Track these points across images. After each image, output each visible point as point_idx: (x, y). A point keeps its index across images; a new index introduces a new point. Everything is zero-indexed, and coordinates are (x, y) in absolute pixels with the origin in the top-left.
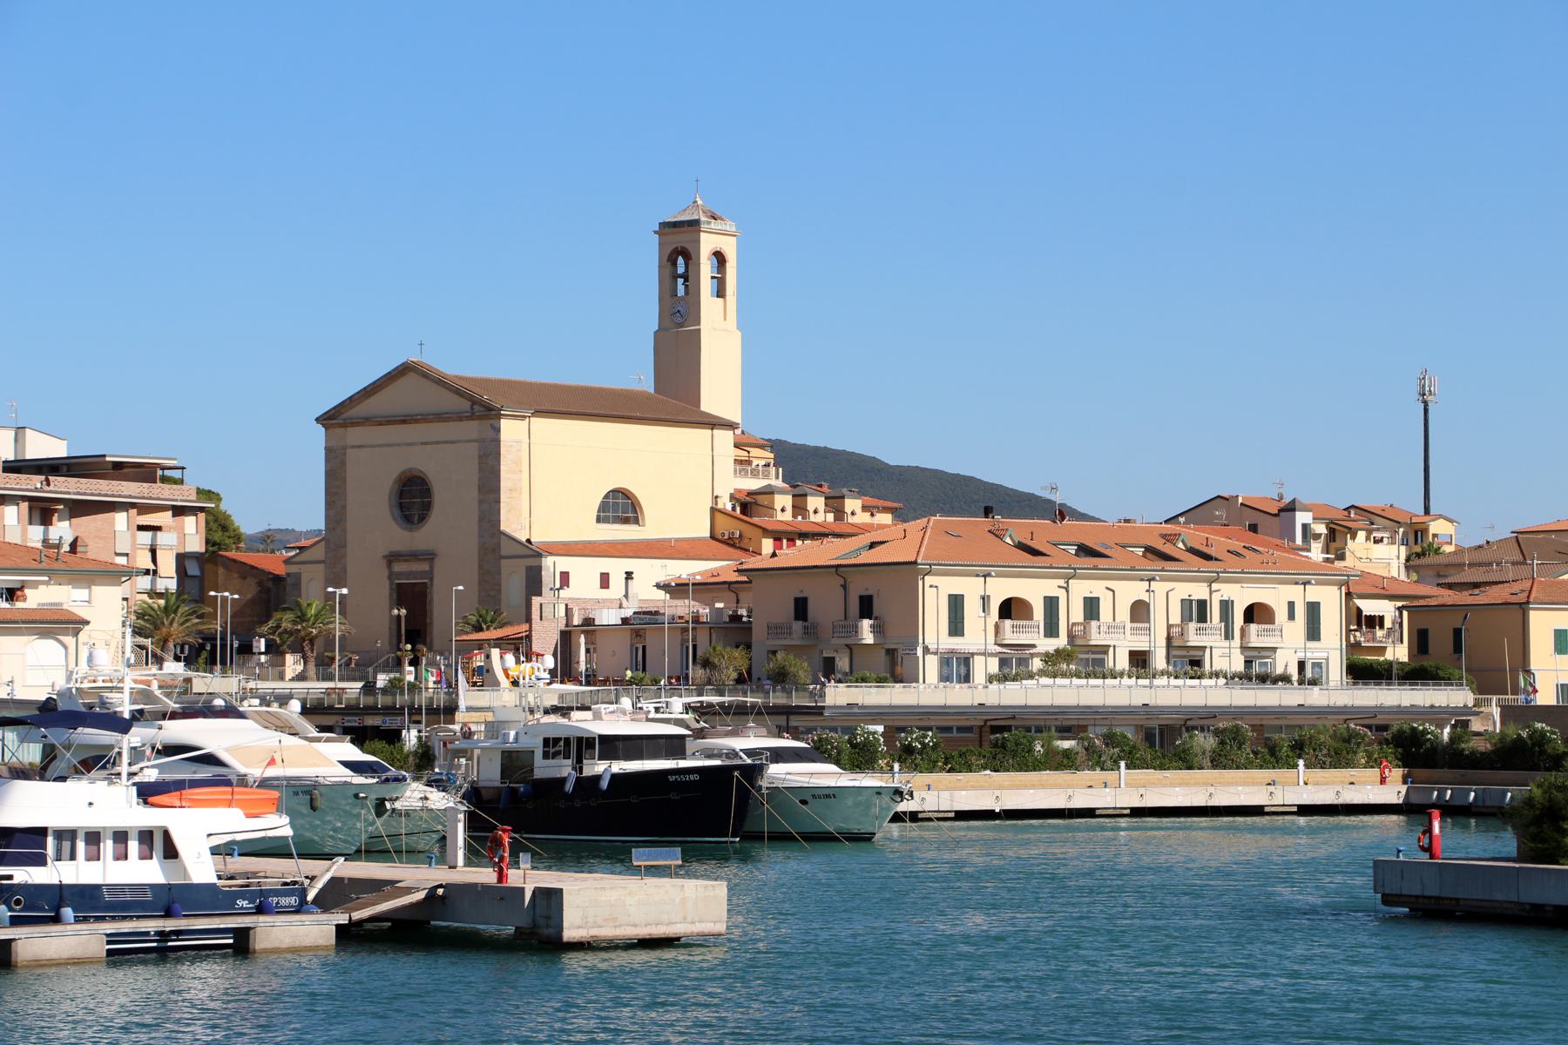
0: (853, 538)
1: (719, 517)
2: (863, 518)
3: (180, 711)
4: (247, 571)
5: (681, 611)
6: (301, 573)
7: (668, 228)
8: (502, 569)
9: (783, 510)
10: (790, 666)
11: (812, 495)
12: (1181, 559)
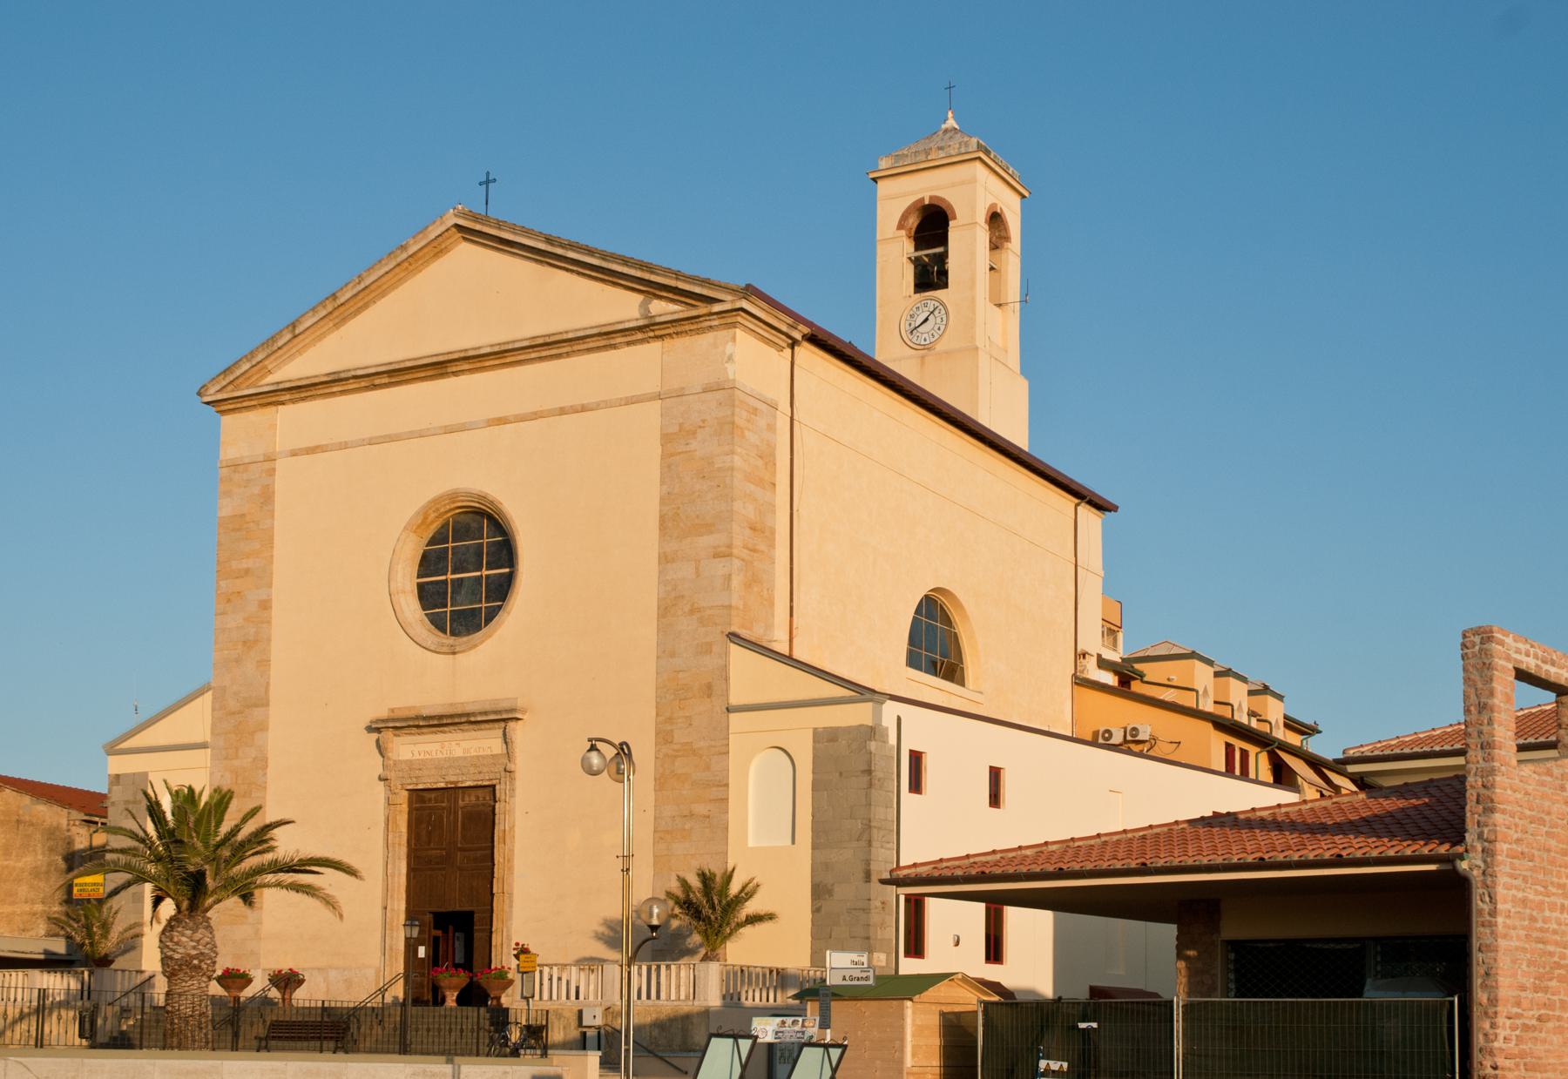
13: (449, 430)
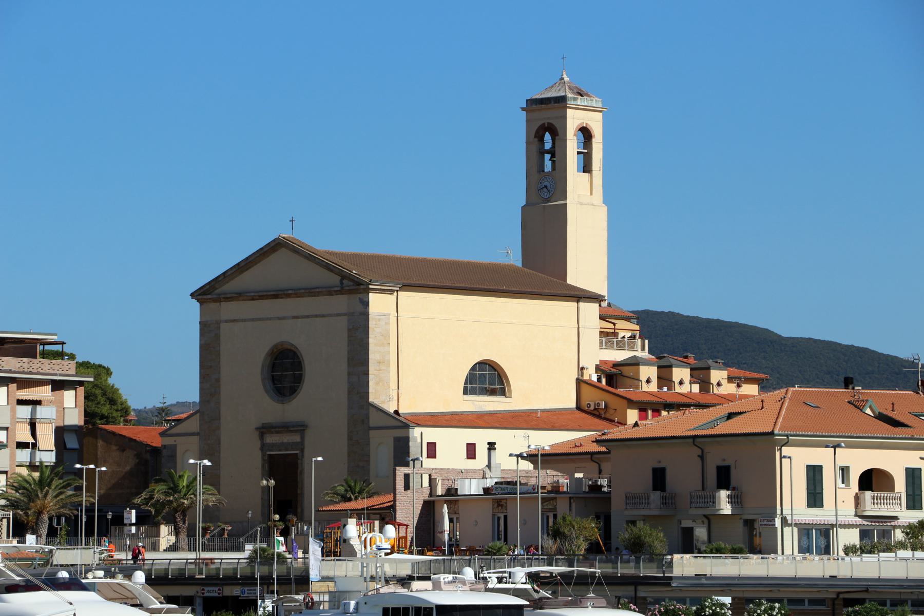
0: (711, 409)
1: (585, 389)
2: (729, 389)
3: (23, 584)
4: (125, 443)
5: (543, 482)
6: (175, 445)
7: (535, 105)
8: (371, 440)
9: (648, 381)
10: (645, 537)
11: (678, 366)
12: (909, 424)
13: (279, 318)
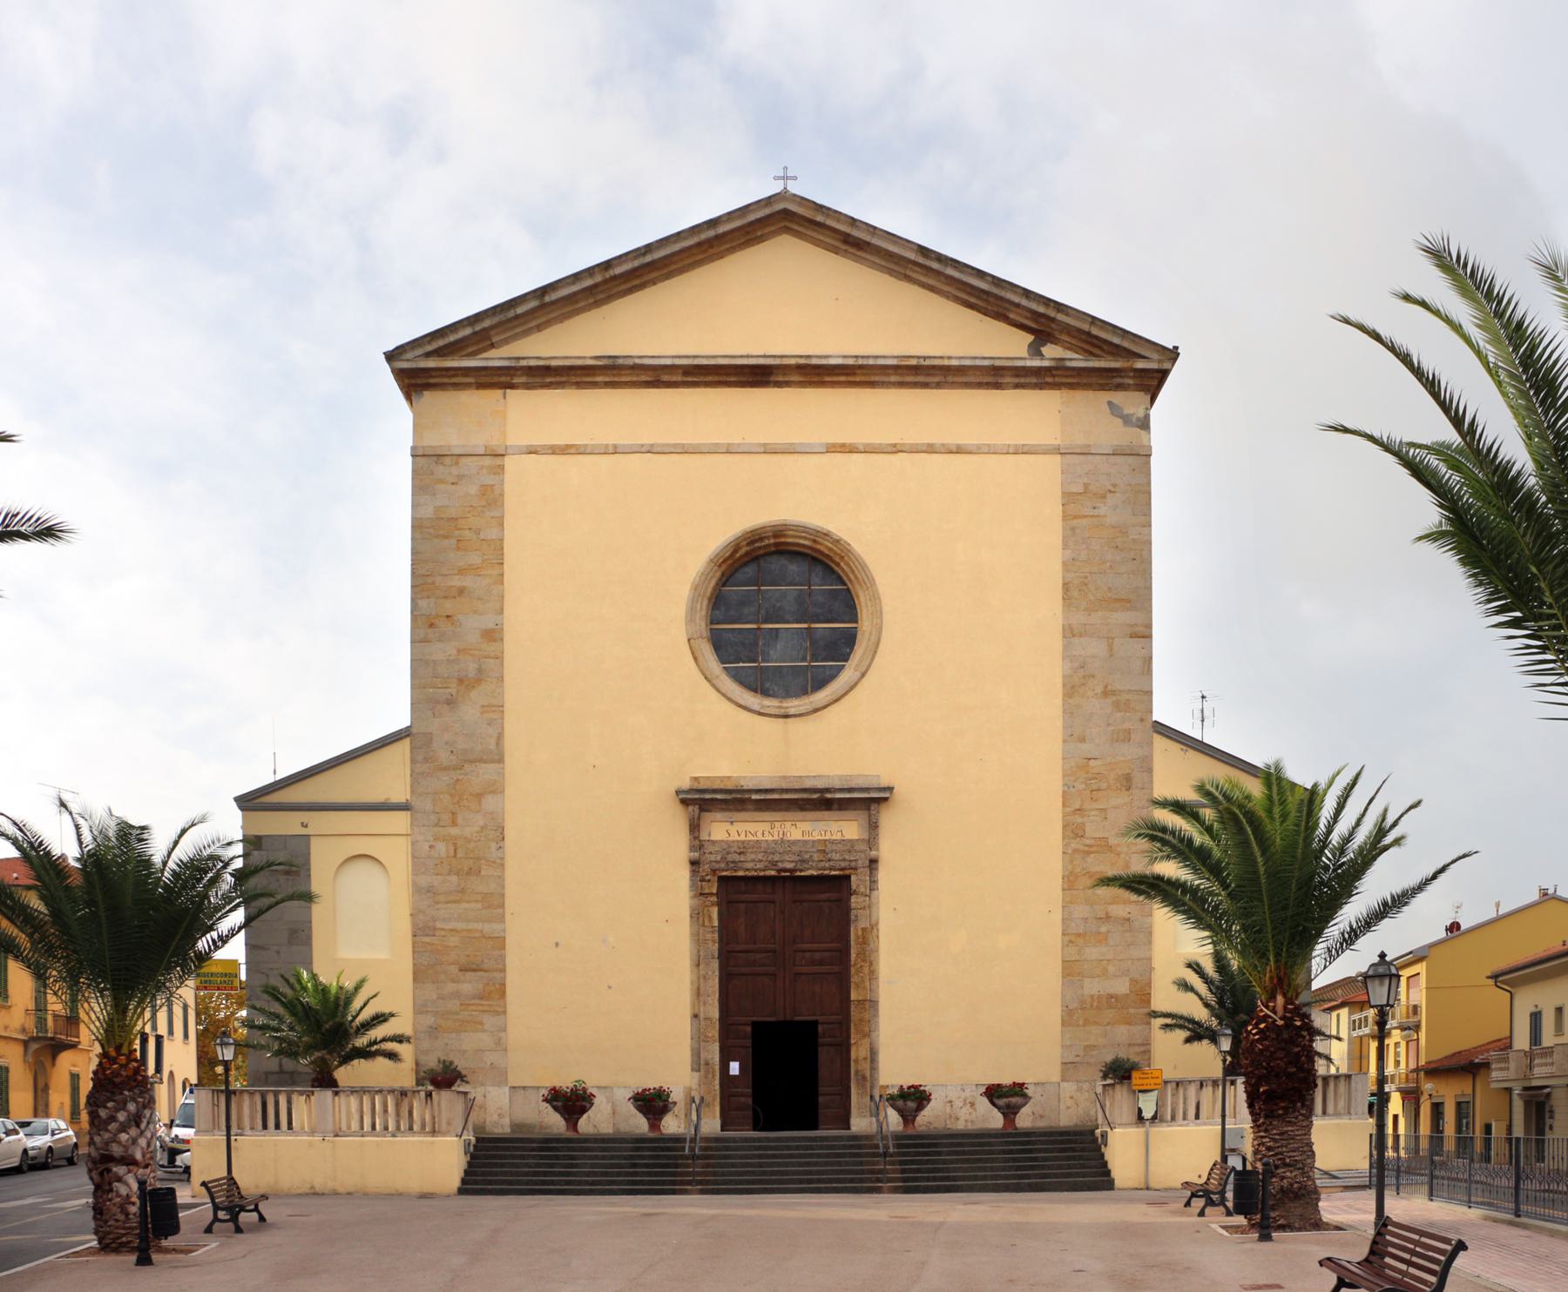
13: (769, 450)
